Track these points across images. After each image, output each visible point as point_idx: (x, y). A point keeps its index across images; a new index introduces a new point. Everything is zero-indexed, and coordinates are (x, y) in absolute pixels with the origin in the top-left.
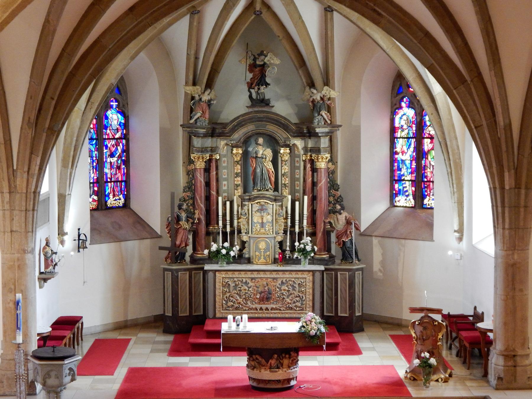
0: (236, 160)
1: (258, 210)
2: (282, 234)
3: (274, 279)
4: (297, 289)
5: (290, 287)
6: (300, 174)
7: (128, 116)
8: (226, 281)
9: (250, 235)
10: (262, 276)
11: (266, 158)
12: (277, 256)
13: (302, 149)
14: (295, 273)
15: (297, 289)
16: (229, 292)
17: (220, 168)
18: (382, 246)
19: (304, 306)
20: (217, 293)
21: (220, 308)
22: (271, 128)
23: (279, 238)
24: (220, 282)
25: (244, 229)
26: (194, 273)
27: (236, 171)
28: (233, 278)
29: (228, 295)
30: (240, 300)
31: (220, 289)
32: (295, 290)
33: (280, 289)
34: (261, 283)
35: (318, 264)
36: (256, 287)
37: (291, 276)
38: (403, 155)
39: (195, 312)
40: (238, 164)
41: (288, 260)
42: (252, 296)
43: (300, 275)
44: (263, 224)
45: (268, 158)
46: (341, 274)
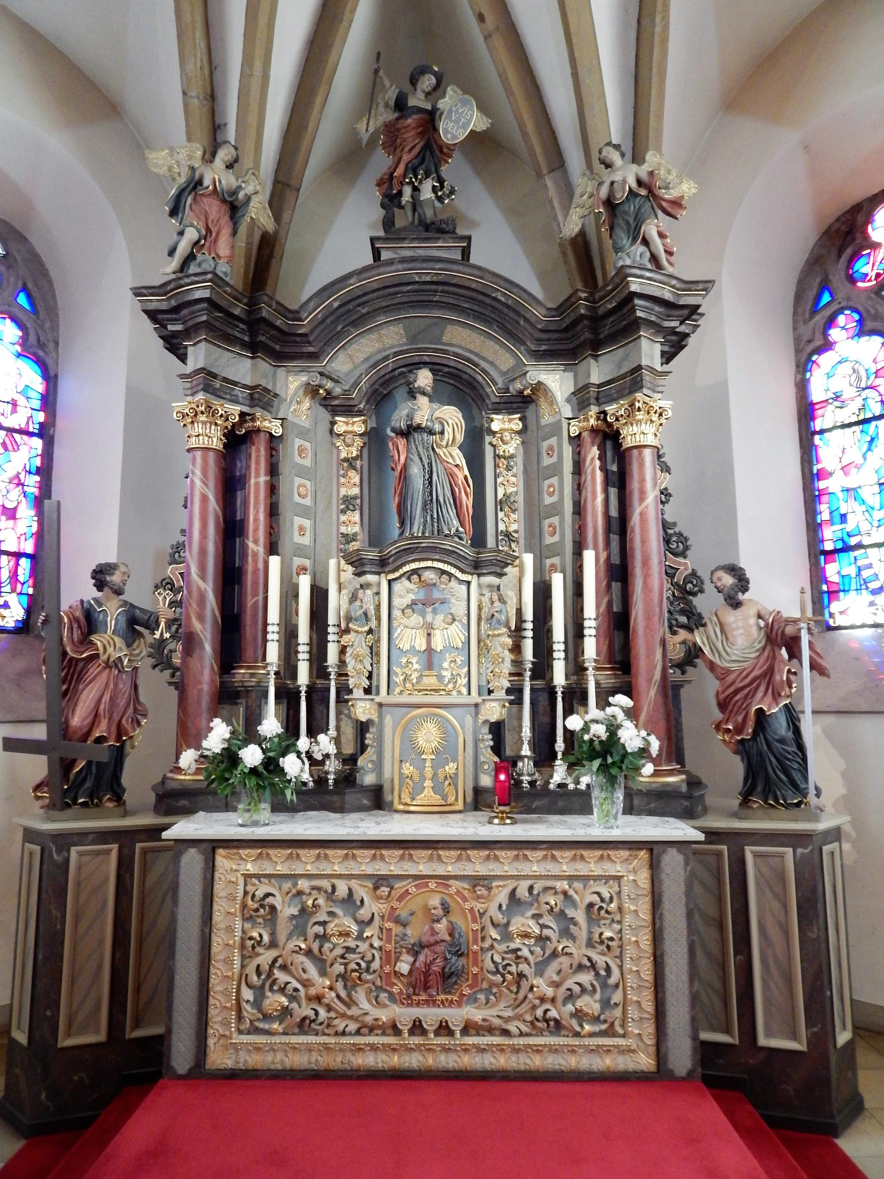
0: (343, 455)
1: (414, 603)
2: (502, 694)
3: (476, 881)
4: (582, 934)
5: (547, 920)
6: (559, 491)
7: (56, 376)
8: (260, 893)
9: (383, 696)
10: (423, 869)
11: (442, 433)
12: (486, 781)
13: (568, 400)
14: (569, 854)
15: (582, 934)
16: (273, 944)
17: (285, 469)
18: (844, 747)
19: (618, 1012)
20: (216, 948)
21: (226, 1023)
22: (464, 339)
23: (494, 711)
24: (232, 898)
25: (359, 673)
26: (144, 852)
27: (343, 491)
28: (295, 877)
29: (265, 957)
30: (321, 983)
31: (230, 930)
32: (573, 938)
33: (504, 929)
34: (415, 904)
35: (651, 813)
36: (397, 921)
37: (551, 868)
38: (846, 474)
39: (136, 1025)
40: (352, 467)
41: (528, 793)
42: (376, 965)
43: (591, 865)
44: (434, 660)
45: (448, 430)
46: (756, 855)
